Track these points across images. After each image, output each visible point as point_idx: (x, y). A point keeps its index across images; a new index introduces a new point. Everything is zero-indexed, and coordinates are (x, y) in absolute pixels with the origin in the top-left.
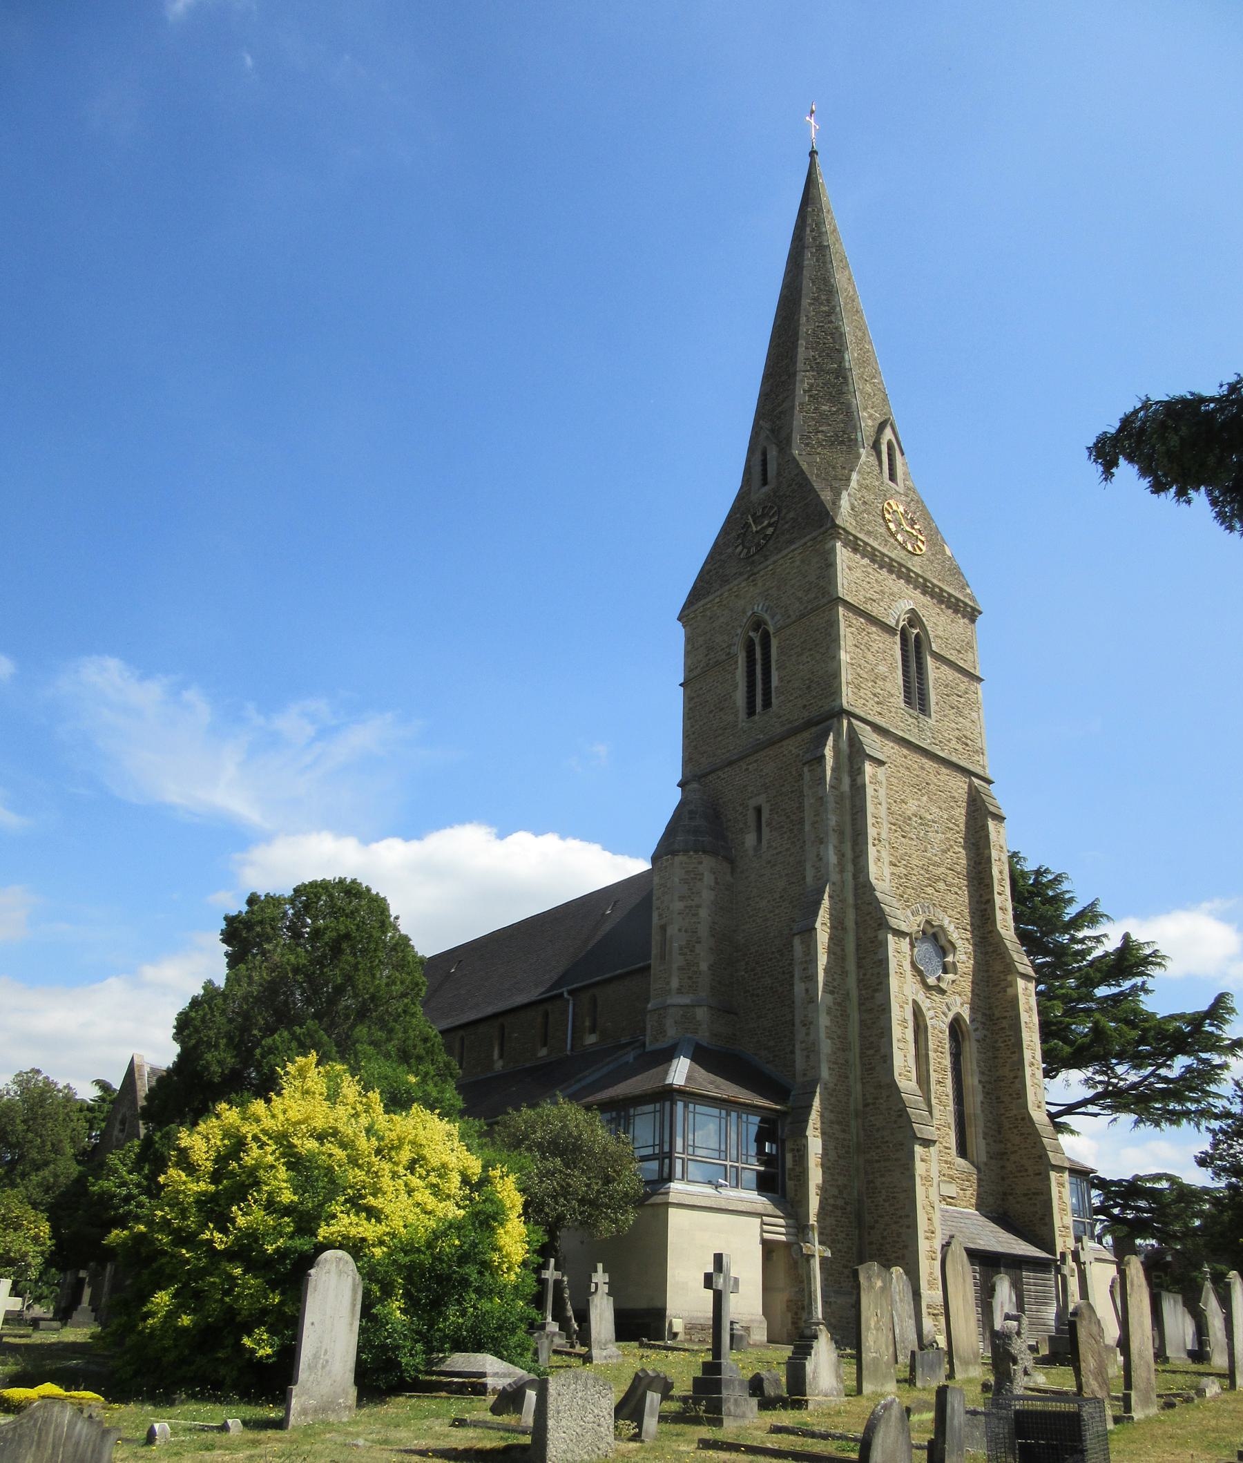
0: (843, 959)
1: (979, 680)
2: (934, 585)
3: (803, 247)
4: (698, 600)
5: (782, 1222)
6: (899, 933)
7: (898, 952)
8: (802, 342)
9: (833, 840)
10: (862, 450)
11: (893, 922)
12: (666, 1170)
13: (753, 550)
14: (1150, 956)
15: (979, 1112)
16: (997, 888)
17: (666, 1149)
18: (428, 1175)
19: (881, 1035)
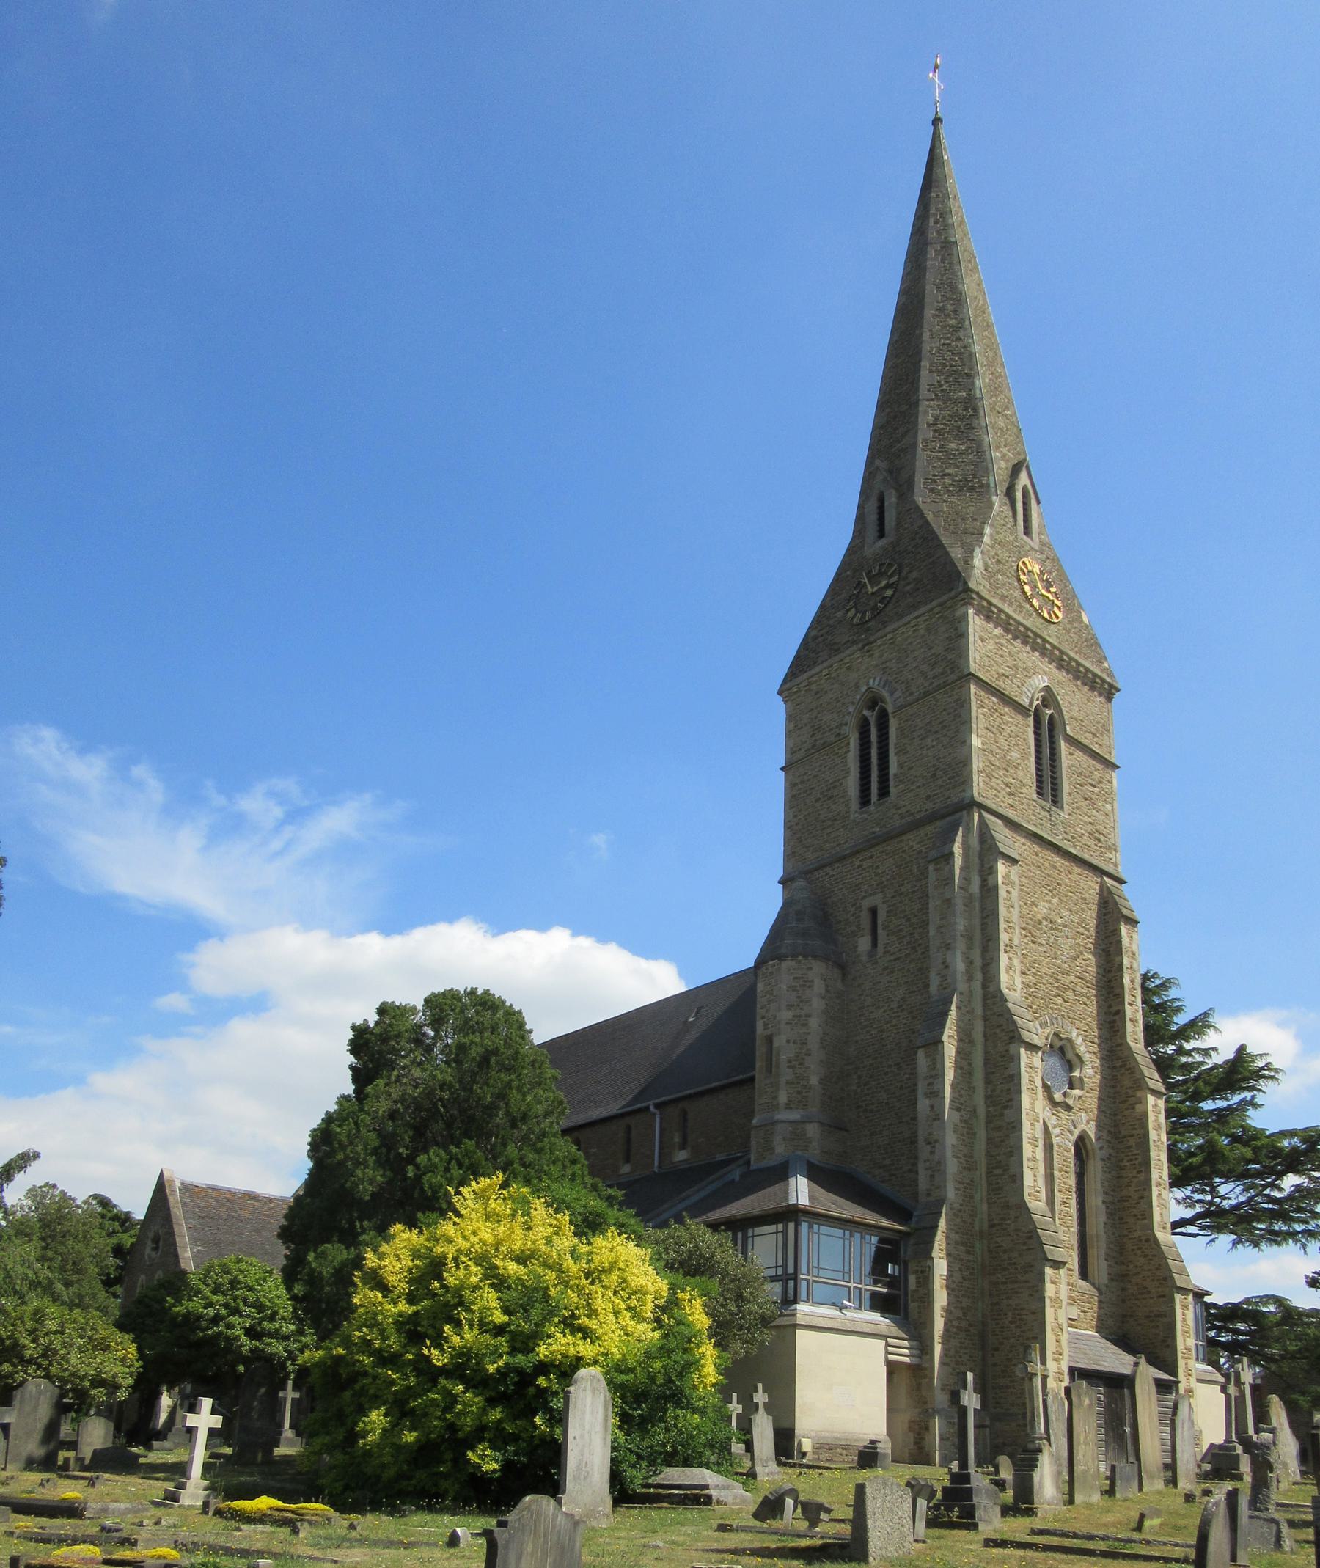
0: (970, 1074)
1: (1114, 767)
2: (1071, 659)
3: (926, 244)
4: (803, 671)
5: (905, 1343)
6: (1032, 1047)
7: (1032, 1068)
8: (925, 364)
9: (961, 945)
10: (994, 498)
11: (1026, 1036)
12: (791, 1292)
13: (869, 615)
14: (1262, 1068)
15: (1102, 1232)
16: (1127, 999)
17: (791, 1270)
18: (629, 1298)
19: (1011, 1154)
